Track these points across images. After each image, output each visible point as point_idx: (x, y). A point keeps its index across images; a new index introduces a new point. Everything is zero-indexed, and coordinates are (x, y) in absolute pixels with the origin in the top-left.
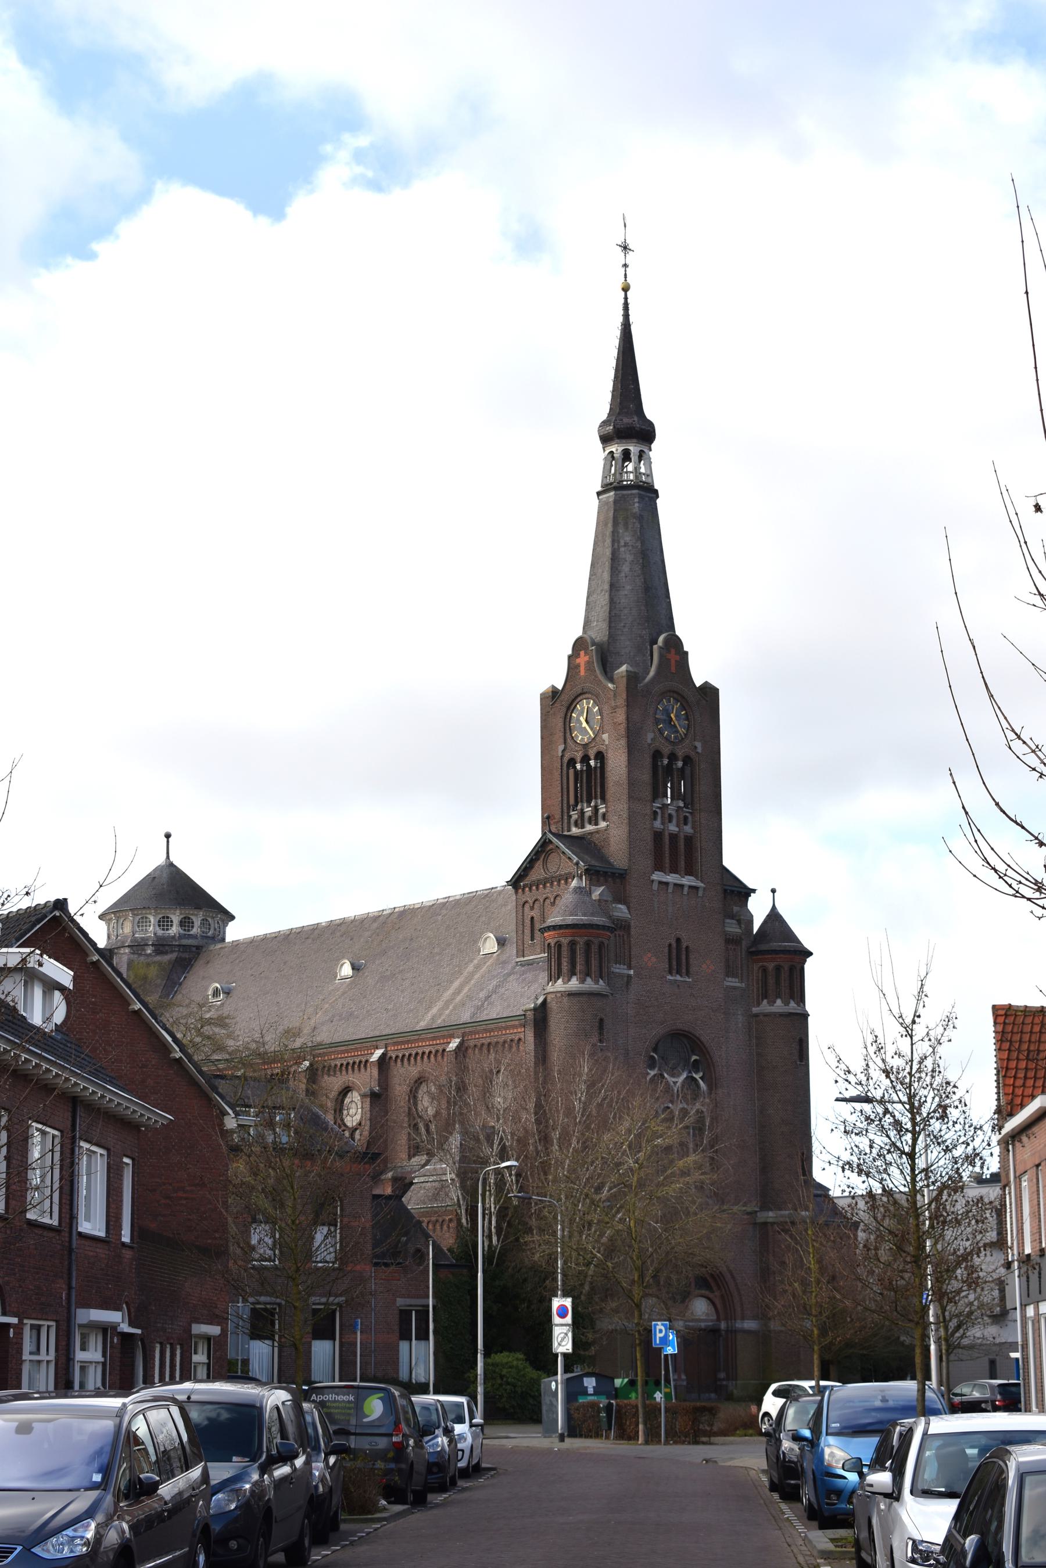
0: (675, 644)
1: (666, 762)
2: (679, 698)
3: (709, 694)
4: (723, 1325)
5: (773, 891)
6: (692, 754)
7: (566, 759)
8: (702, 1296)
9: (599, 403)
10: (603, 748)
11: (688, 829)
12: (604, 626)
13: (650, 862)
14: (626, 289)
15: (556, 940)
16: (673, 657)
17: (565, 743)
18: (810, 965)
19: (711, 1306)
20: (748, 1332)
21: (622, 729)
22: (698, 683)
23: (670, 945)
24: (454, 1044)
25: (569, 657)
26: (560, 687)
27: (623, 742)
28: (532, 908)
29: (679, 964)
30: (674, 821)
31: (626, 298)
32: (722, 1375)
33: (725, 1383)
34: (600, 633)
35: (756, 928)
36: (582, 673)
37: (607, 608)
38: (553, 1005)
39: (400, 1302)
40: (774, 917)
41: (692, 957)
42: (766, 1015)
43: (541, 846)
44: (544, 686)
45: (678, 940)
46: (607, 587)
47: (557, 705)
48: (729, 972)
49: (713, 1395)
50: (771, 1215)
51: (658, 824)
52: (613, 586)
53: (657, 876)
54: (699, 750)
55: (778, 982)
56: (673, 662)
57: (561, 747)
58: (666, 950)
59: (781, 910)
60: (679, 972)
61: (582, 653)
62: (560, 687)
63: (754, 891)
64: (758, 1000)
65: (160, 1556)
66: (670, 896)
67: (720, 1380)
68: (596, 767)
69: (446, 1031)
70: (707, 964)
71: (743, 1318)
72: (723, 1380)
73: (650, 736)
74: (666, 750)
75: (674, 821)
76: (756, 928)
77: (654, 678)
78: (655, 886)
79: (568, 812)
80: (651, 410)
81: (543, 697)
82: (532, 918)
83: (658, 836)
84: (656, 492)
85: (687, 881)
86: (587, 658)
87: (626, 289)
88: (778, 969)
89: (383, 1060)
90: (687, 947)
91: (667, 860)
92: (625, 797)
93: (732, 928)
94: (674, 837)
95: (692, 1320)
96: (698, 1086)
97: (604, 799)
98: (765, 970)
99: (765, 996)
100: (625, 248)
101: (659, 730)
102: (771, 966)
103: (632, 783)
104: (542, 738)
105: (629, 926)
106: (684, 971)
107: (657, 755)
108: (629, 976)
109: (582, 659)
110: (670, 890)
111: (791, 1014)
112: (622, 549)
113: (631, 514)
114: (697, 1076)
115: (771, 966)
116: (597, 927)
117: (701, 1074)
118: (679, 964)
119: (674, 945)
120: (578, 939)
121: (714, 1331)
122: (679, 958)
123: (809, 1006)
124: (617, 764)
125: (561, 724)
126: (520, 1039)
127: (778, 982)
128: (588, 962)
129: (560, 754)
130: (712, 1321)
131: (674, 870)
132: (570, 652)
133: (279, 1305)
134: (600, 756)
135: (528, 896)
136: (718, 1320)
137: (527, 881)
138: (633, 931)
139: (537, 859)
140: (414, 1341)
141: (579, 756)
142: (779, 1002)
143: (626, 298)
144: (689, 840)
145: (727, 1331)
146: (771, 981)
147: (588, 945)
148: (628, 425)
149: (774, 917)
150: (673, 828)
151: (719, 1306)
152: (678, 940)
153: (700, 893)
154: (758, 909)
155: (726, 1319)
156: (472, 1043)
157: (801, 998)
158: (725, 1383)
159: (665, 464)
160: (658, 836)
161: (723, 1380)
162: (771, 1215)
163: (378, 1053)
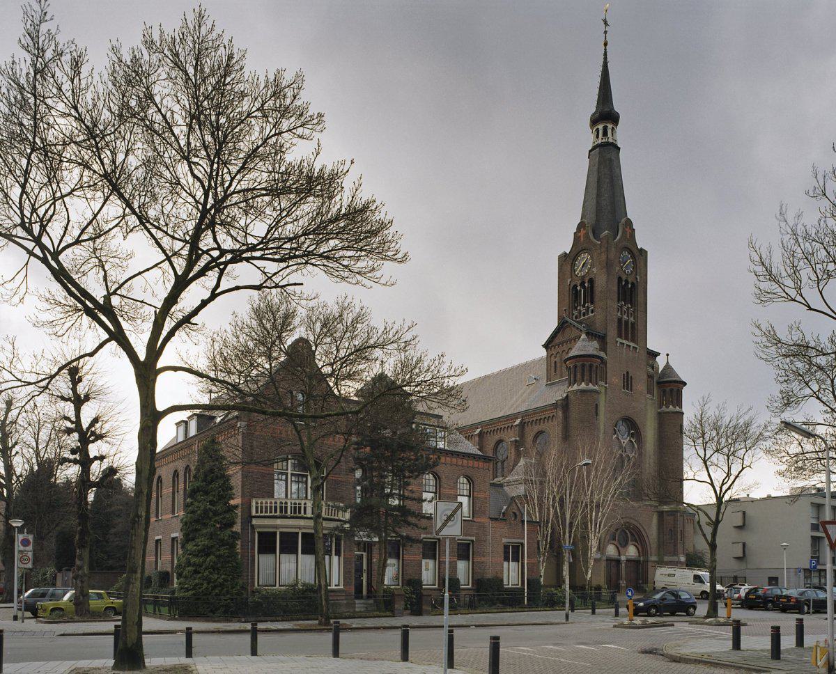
1: (623, 283)
3: (643, 253)
4: (641, 559)
5: (668, 355)
6: (635, 282)
7: (572, 286)
8: (636, 546)
9: (591, 107)
10: (592, 276)
12: (593, 216)
13: (616, 335)
14: (606, 44)
16: (629, 231)
17: (571, 277)
18: (685, 391)
19: (636, 550)
24: (518, 422)
25: (575, 233)
26: (568, 252)
28: (555, 357)
29: (628, 385)
31: (605, 49)
34: (591, 220)
35: (660, 371)
36: (582, 239)
37: (594, 207)
38: (572, 397)
39: (504, 540)
40: (668, 366)
41: (633, 381)
42: (664, 413)
44: (561, 252)
46: (595, 196)
47: (567, 261)
50: (666, 508)
52: (598, 196)
53: (618, 339)
61: (582, 229)
62: (568, 252)
68: (588, 288)
69: (513, 417)
70: (640, 386)
73: (617, 268)
74: (624, 278)
76: (660, 371)
80: (618, 106)
81: (560, 257)
82: (555, 362)
83: (620, 320)
84: (619, 149)
85: (632, 344)
87: (606, 44)
89: (480, 435)
96: (634, 445)
97: (592, 302)
100: (606, 23)
104: (559, 278)
107: (620, 279)
109: (583, 232)
110: (625, 347)
112: (603, 176)
114: (633, 441)
118: (628, 385)
122: (628, 382)
123: (684, 410)
124: (601, 282)
125: (569, 269)
126: (553, 416)
131: (626, 339)
132: (575, 231)
134: (591, 281)
135: (553, 351)
137: (553, 344)
139: (558, 332)
140: (511, 562)
141: (579, 283)
142: (671, 407)
143: (605, 49)
145: (643, 561)
148: (605, 116)
149: (668, 366)
151: (640, 550)
154: (661, 362)
155: (643, 556)
156: (527, 421)
159: (622, 135)
162: (666, 508)
163: (478, 430)
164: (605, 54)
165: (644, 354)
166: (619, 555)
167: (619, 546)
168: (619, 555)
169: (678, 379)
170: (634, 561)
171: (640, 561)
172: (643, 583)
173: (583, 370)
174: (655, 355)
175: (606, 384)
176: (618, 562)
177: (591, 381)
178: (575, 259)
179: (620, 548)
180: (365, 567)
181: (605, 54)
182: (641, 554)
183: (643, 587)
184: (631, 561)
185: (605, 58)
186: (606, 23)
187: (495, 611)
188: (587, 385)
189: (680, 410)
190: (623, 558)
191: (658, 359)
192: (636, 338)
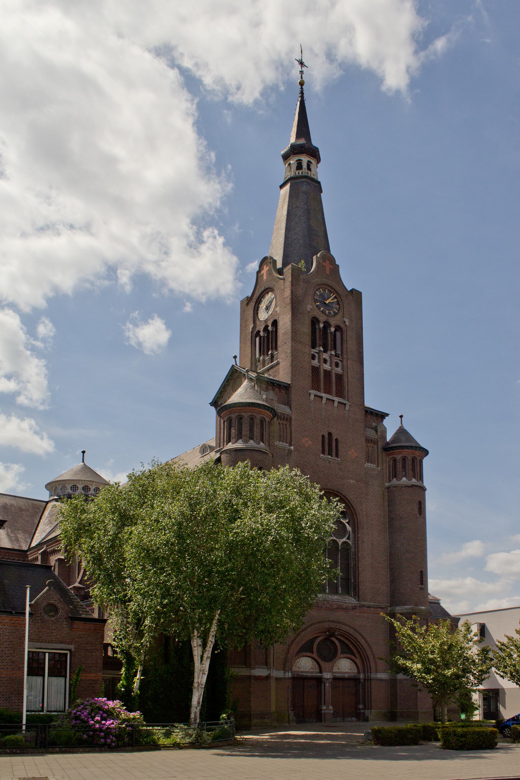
0: (329, 259)
1: (322, 325)
2: (332, 290)
3: (356, 296)
4: (362, 676)
5: (401, 417)
6: (342, 326)
10: (276, 318)
11: (339, 370)
15: (228, 417)
16: (328, 266)
18: (426, 461)
20: (381, 680)
21: (288, 301)
22: (349, 289)
23: (323, 436)
27: (289, 307)
30: (328, 363)
31: (302, 88)
32: (361, 706)
33: (362, 711)
40: (402, 432)
43: (230, 376)
45: (330, 434)
48: (369, 460)
49: (354, 719)
51: (315, 363)
54: (347, 324)
55: (404, 467)
56: (328, 269)
57: (252, 326)
58: (320, 438)
59: (406, 427)
60: (330, 454)
63: (387, 415)
64: (389, 478)
65: (356, 735)
66: (324, 405)
67: (359, 709)
68: (272, 331)
71: (376, 672)
72: (362, 709)
74: (322, 318)
75: (328, 363)
77: (314, 270)
78: (312, 397)
79: (255, 364)
83: (315, 370)
85: (337, 399)
86: (268, 268)
88: (404, 459)
90: (337, 440)
91: (322, 384)
92: (289, 340)
93: (371, 433)
94: (327, 374)
95: (339, 673)
98: (395, 460)
99: (395, 476)
100: (301, 63)
101: (322, 311)
102: (399, 457)
103: (294, 331)
105: (291, 419)
106: (334, 453)
107: (315, 321)
108: (290, 451)
111: (413, 486)
113: (305, 192)
114: (344, 521)
115: (399, 457)
116: (259, 405)
117: (347, 521)
119: (326, 436)
120: (243, 414)
121: (355, 680)
123: (426, 483)
127: (404, 467)
128: (251, 431)
129: (251, 330)
130: (353, 673)
133: (70, 650)
136: (359, 672)
138: (293, 422)
143: (302, 88)
144: (339, 377)
146: (399, 466)
147: (252, 419)
149: (402, 432)
150: (327, 367)
151: (360, 665)
152: (330, 434)
153: (347, 408)
154: (391, 427)
157: (421, 478)
158: (362, 711)
160: (315, 370)
161: (362, 709)
164: (302, 93)
165: (360, 415)
166: (321, 672)
167: (319, 660)
168: (321, 672)
169: (413, 444)
170: (349, 679)
171: (359, 679)
172: (365, 709)
173: (240, 424)
174: (382, 416)
175: (291, 445)
176: (319, 680)
177: (251, 438)
178: (259, 301)
179: (322, 663)
180: (361, 699)
181: (302, 93)
182: (361, 670)
183: (364, 713)
184: (343, 679)
185: (302, 97)
186: (301, 63)
187: (237, 753)
188: (246, 442)
189: (419, 484)
190: (327, 675)
191: (386, 422)
192: (346, 393)
